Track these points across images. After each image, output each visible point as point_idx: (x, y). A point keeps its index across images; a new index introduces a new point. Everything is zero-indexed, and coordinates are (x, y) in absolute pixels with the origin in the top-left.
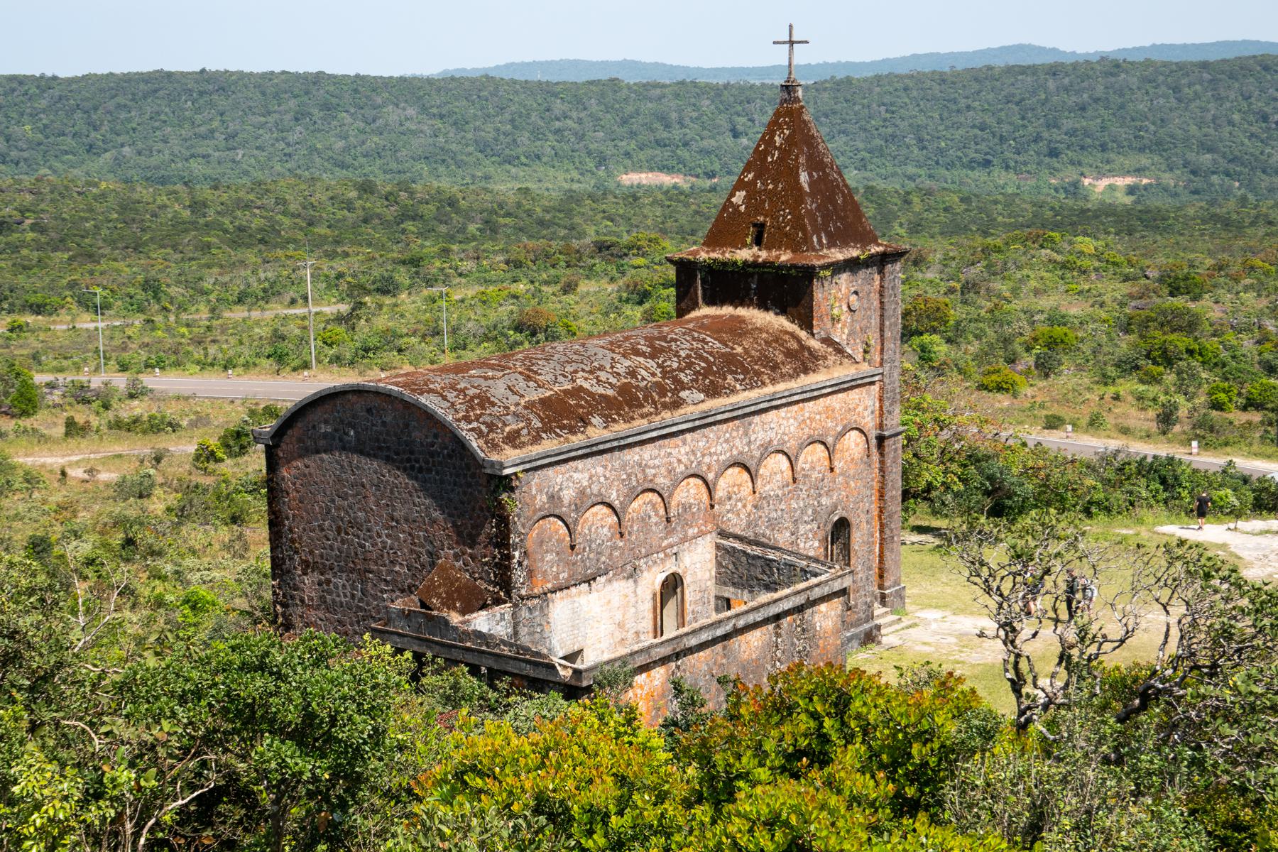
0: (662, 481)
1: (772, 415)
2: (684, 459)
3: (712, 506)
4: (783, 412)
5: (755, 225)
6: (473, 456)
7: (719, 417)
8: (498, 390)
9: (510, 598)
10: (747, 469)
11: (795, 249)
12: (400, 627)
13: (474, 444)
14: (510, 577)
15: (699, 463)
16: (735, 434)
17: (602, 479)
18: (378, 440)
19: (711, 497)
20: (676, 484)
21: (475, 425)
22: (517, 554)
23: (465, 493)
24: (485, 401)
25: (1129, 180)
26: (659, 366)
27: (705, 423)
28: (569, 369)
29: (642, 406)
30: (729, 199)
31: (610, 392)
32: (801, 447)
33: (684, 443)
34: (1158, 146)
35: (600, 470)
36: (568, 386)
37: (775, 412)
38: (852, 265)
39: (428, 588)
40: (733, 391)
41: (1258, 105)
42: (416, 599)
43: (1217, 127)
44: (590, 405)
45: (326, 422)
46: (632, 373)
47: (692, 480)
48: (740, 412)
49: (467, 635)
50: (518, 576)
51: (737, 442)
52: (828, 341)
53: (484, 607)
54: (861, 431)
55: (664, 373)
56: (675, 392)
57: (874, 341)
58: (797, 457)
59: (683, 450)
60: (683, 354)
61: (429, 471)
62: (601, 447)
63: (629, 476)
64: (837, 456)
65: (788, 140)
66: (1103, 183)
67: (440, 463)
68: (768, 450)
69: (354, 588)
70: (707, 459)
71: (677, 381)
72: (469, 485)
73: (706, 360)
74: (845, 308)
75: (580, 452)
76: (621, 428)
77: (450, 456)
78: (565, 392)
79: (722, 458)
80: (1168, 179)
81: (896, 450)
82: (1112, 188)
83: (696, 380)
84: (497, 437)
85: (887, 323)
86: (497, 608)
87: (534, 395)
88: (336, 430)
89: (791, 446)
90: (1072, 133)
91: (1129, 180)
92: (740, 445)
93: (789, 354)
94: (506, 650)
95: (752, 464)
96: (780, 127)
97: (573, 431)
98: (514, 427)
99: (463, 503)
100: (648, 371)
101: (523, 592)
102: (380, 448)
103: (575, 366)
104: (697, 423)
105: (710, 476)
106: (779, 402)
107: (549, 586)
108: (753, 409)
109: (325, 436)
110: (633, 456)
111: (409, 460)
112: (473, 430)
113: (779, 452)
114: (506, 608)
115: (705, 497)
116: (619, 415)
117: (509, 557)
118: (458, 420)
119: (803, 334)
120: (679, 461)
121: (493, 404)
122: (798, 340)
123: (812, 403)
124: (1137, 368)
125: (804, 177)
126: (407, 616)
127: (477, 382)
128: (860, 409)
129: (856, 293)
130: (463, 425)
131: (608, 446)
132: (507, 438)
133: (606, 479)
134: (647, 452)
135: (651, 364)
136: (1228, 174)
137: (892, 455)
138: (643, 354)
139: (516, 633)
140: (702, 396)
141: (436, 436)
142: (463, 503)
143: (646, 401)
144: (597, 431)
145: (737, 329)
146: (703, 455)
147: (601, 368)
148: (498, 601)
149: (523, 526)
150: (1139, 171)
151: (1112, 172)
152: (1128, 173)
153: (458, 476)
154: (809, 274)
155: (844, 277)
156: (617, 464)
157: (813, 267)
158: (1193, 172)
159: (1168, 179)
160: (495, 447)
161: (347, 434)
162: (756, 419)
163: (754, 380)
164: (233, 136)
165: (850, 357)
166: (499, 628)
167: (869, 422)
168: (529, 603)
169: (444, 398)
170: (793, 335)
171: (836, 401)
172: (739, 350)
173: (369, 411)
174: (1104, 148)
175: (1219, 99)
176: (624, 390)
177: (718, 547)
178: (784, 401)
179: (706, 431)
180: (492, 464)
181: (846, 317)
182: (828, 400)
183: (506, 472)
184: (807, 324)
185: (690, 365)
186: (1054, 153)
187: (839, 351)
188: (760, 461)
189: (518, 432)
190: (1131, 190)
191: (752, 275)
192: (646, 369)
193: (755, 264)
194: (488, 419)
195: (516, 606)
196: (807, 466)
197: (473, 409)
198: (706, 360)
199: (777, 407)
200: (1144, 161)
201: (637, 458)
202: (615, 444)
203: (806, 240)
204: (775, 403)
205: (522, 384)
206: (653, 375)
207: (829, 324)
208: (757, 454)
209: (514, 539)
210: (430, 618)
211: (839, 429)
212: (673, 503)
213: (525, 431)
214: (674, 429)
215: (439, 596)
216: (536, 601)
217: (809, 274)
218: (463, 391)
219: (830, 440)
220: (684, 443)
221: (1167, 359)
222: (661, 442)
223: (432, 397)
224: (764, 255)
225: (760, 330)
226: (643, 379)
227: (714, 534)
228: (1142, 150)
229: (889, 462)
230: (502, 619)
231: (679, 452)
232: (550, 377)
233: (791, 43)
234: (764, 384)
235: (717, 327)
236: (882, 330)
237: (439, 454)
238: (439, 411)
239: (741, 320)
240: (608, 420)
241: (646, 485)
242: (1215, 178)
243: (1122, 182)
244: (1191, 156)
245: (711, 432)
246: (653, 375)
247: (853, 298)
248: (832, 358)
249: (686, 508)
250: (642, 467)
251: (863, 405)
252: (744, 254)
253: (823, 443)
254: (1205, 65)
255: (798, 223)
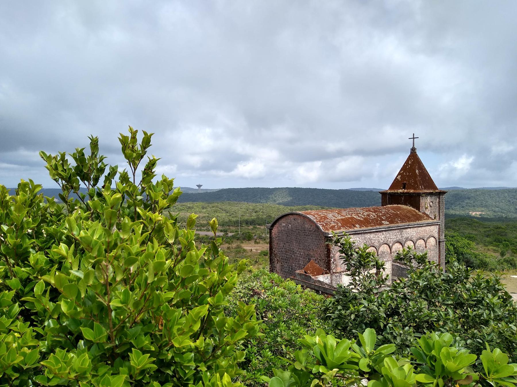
0: (376, 244)
1: (409, 230)
2: (383, 239)
3: (391, 253)
4: (412, 229)
5: (403, 184)
6: (321, 231)
7: (393, 228)
8: (330, 216)
9: (330, 272)
10: (401, 244)
11: (414, 189)
12: (298, 277)
13: (321, 228)
14: (330, 266)
15: (387, 241)
16: (398, 234)
17: (358, 242)
18: (296, 227)
19: (391, 251)
20: (380, 246)
21: (322, 223)
22: (332, 260)
23: (318, 242)
24: (325, 218)
25: (480, 213)
26: (376, 214)
27: (388, 230)
28: (350, 213)
29: (371, 224)
30: (396, 178)
31: (362, 219)
32: (417, 240)
33: (383, 234)
34: (486, 206)
35: (358, 239)
36: (350, 216)
37: (409, 229)
38: (431, 194)
39: (307, 268)
40: (397, 223)
41: (508, 199)
42: (304, 271)
43: (499, 203)
44: (356, 222)
45: (284, 223)
46: (368, 215)
47: (385, 245)
48: (399, 228)
49: (315, 281)
50: (333, 266)
51: (398, 236)
52: (424, 213)
53: (323, 274)
54: (434, 238)
55: (378, 216)
56: (381, 221)
57: (437, 214)
58: (416, 243)
59: (382, 236)
60: (383, 212)
61: (309, 236)
62: (358, 232)
63: (366, 241)
64: (428, 244)
65: (412, 162)
66: (474, 214)
67: (312, 233)
68: (407, 239)
69: (289, 268)
70: (389, 240)
71: (381, 218)
72: (320, 240)
73: (389, 214)
74: (429, 206)
75: (352, 233)
76: (364, 228)
77: (315, 231)
78: (349, 218)
79: (394, 240)
80: (488, 213)
81: (443, 245)
82: (476, 214)
83: (387, 219)
84: (328, 227)
85: (441, 211)
86: (326, 275)
87: (340, 218)
88: (286, 225)
89: (414, 239)
90: (467, 203)
91: (480, 213)
92: (399, 237)
93: (413, 215)
94: (327, 287)
95: (403, 243)
96: (411, 159)
97: (350, 228)
98: (333, 225)
99: (318, 245)
100: (373, 215)
101: (334, 271)
102: (297, 229)
103: (352, 212)
104: (387, 229)
105: (391, 245)
106: (411, 226)
107: (342, 270)
108: (403, 227)
109: (284, 226)
110: (368, 236)
111: (304, 233)
112: (321, 224)
113: (411, 240)
114: (329, 275)
115: (389, 250)
116: (364, 225)
117: (330, 261)
118: (317, 221)
119: (417, 211)
120: (381, 239)
121: (328, 219)
122: (416, 212)
123: (420, 228)
124: (492, 243)
125: (417, 171)
126: (300, 275)
127: (324, 213)
128: (434, 231)
129: (432, 202)
130: (318, 223)
131: (360, 232)
132: (331, 227)
133: (360, 241)
134: (372, 236)
135: (374, 214)
136: (501, 212)
137: (442, 247)
138: (372, 212)
139: (331, 283)
140: (388, 223)
141: (311, 226)
142: (318, 245)
143: (372, 222)
144: (357, 228)
145: (399, 209)
146: (389, 239)
147: (360, 213)
148: (326, 273)
149: (334, 252)
150: (482, 211)
151: (476, 211)
152: (480, 211)
153: (317, 237)
154: (419, 195)
155: (429, 198)
156: (363, 238)
157: (420, 193)
158: (494, 212)
159: (488, 213)
160: (327, 229)
161: (289, 226)
162: (404, 230)
163: (402, 221)
164: (299, 199)
165: (431, 218)
166: (326, 281)
167: (436, 236)
168: (336, 274)
169: (314, 216)
170: (414, 211)
171: (428, 228)
172: (398, 213)
173: (294, 219)
174: (474, 206)
175: (499, 197)
176: (365, 219)
177: (393, 265)
178: (412, 226)
179: (390, 232)
180: (326, 233)
181: (429, 208)
182: (425, 228)
183: (330, 236)
184: (418, 208)
185: (385, 215)
186: (463, 207)
187: (427, 216)
188: (405, 242)
189: (334, 226)
190: (480, 215)
191: (402, 196)
192: (372, 215)
193: (403, 193)
194: (326, 222)
195: (332, 275)
196: (419, 245)
197: (322, 219)
198: (389, 214)
199: (410, 228)
200: (483, 209)
201: (369, 237)
202: (363, 232)
203: (418, 187)
204: (409, 226)
205: (337, 215)
206: (374, 216)
207: (424, 209)
208: (404, 240)
209: (331, 255)
210: (306, 276)
211: (428, 236)
212: (380, 251)
213: (336, 226)
214: (380, 230)
215: (310, 270)
216: (338, 274)
217: (419, 195)
218: (320, 215)
219: (425, 239)
220: (383, 234)
221: (500, 241)
222: (376, 233)
223: (311, 215)
224: (406, 191)
225: (405, 209)
226: (371, 217)
227: (392, 261)
228: (482, 207)
229: (441, 248)
230: (327, 278)
231: (381, 237)
232: (345, 214)
233: (414, 138)
234: (406, 222)
235: (393, 209)
236: (439, 213)
237: (312, 231)
238: (312, 219)
239: (400, 207)
240: (361, 226)
241: (371, 245)
242: (499, 213)
243: (478, 213)
244: (493, 208)
245: (390, 232)
246: (374, 216)
247: (431, 203)
248: (426, 217)
249: (383, 253)
250: (371, 240)
251: (434, 230)
252: (400, 191)
253: (424, 240)
254: (496, 191)
255: (416, 183)
